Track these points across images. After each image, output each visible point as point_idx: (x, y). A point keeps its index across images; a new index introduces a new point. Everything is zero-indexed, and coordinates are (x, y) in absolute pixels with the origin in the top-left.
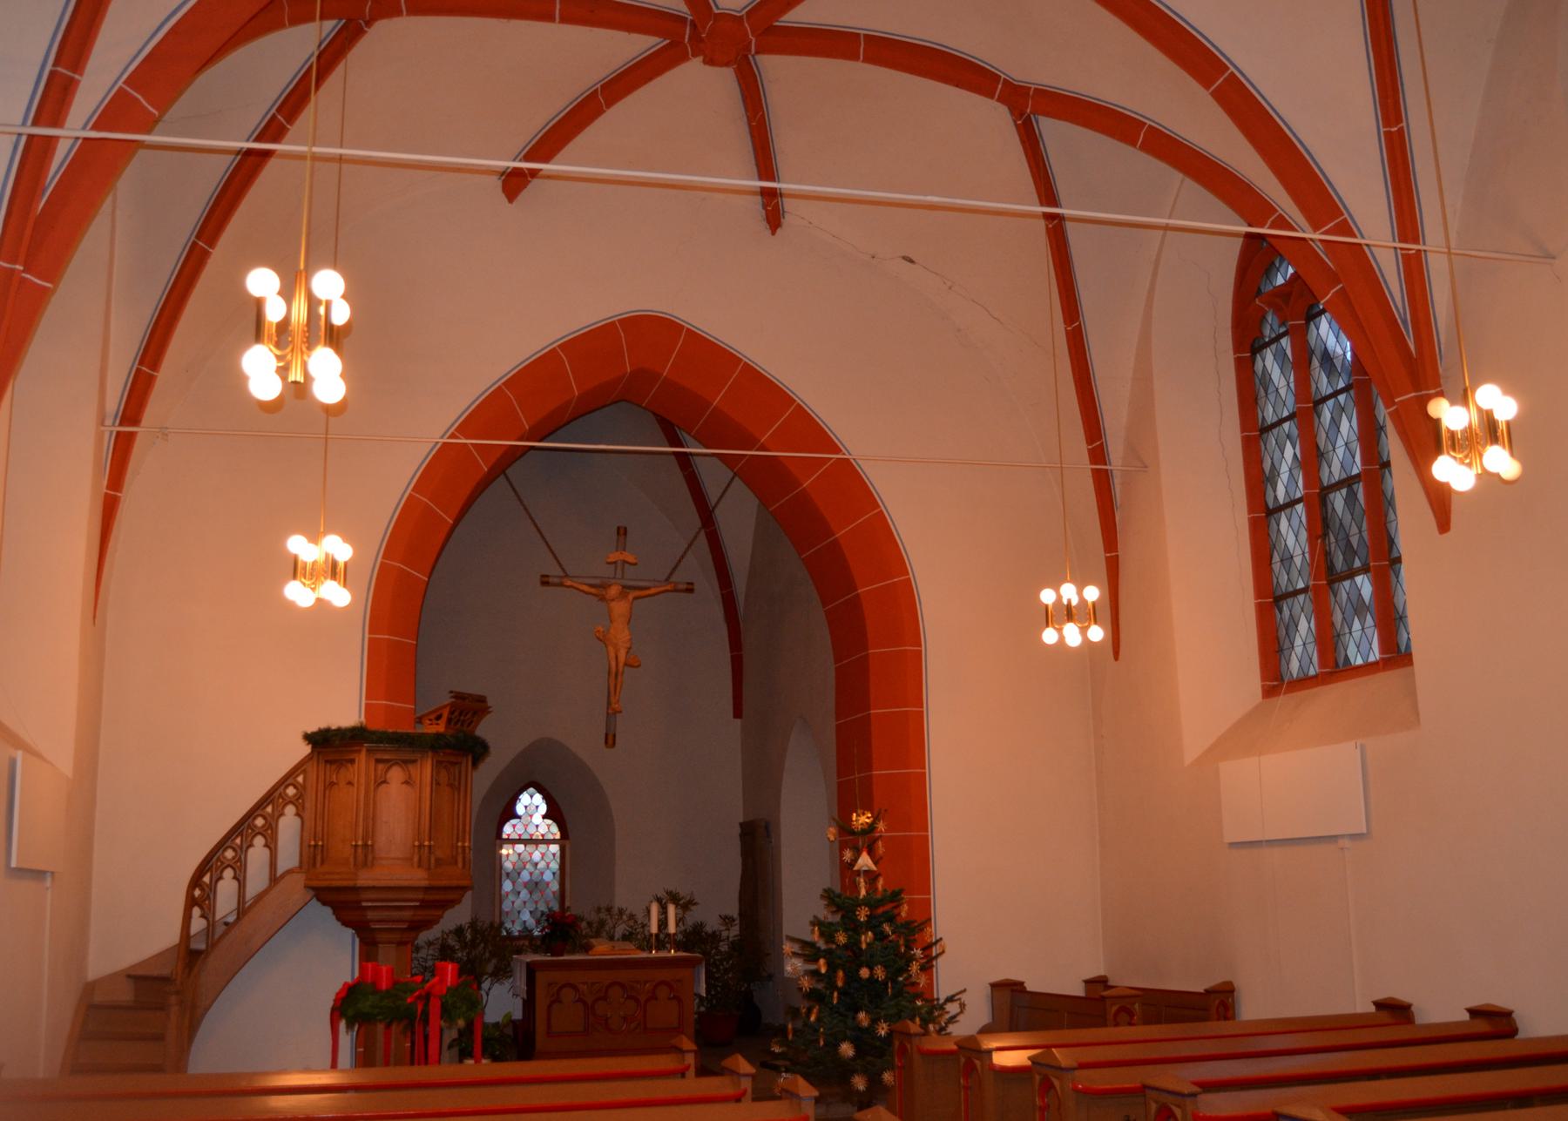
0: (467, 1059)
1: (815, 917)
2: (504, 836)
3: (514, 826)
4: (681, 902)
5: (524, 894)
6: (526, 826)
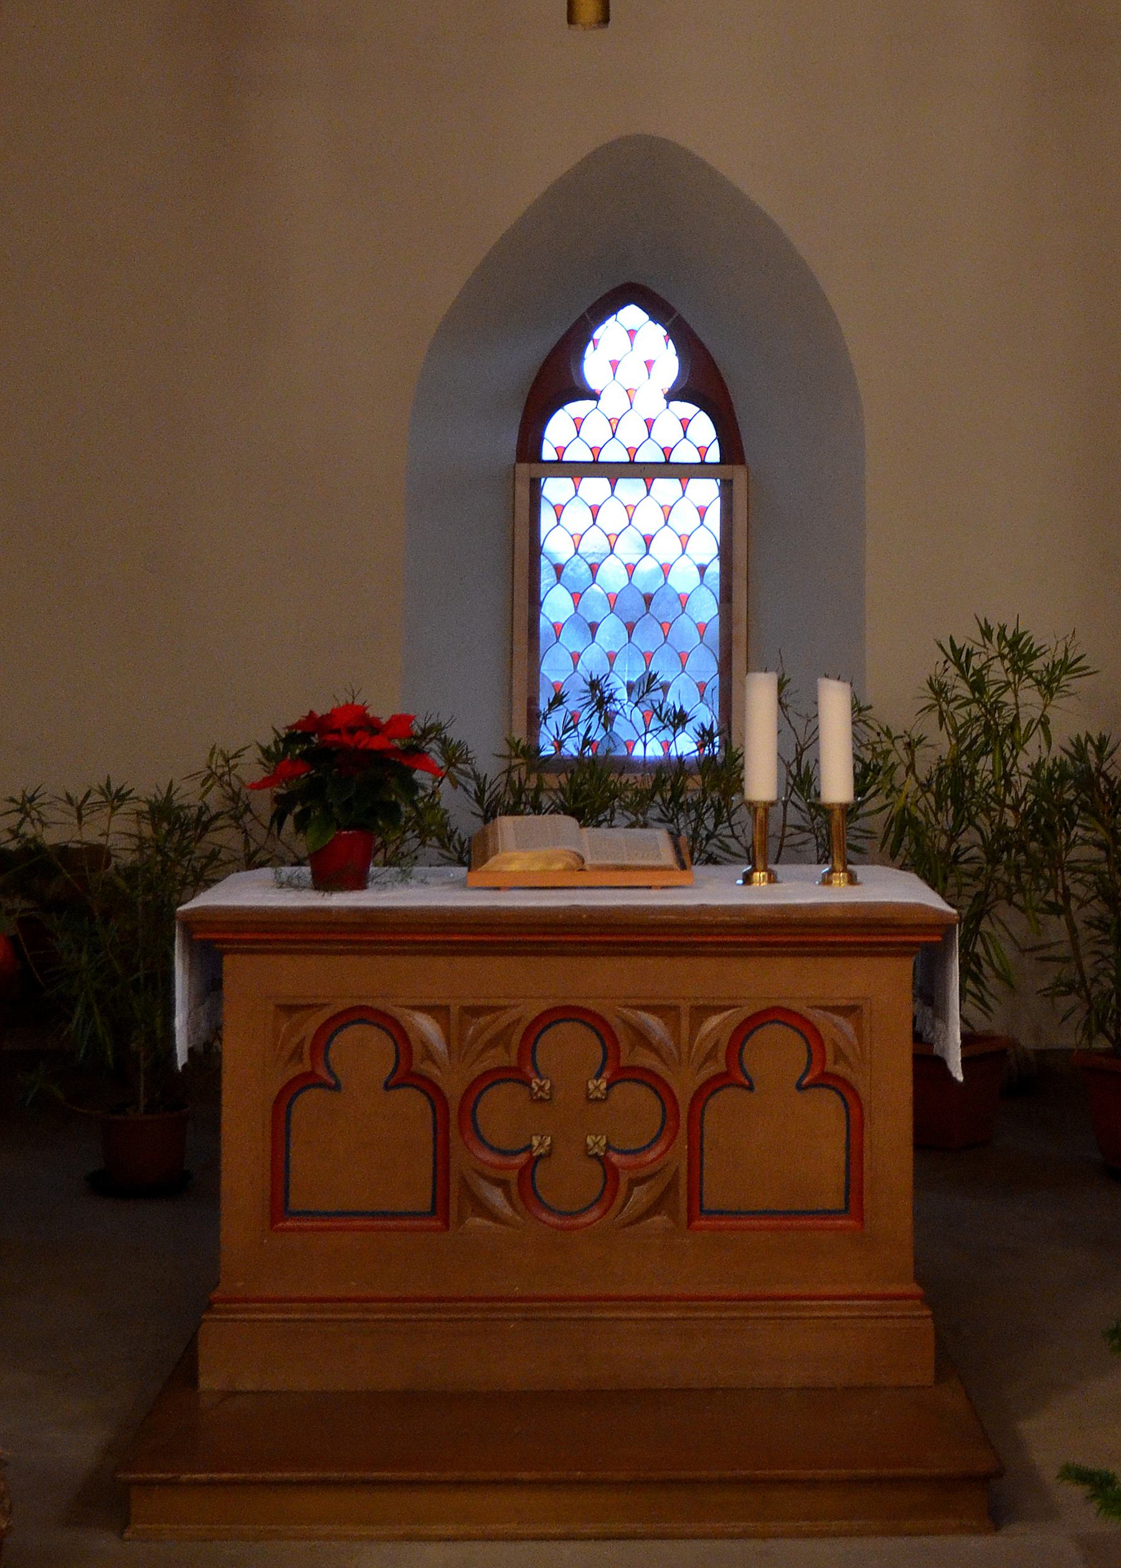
0: (593, 332)
1: (311, 712)
2: (548, 454)
3: (578, 423)
4: (1037, 665)
5: (611, 631)
6: (614, 424)
